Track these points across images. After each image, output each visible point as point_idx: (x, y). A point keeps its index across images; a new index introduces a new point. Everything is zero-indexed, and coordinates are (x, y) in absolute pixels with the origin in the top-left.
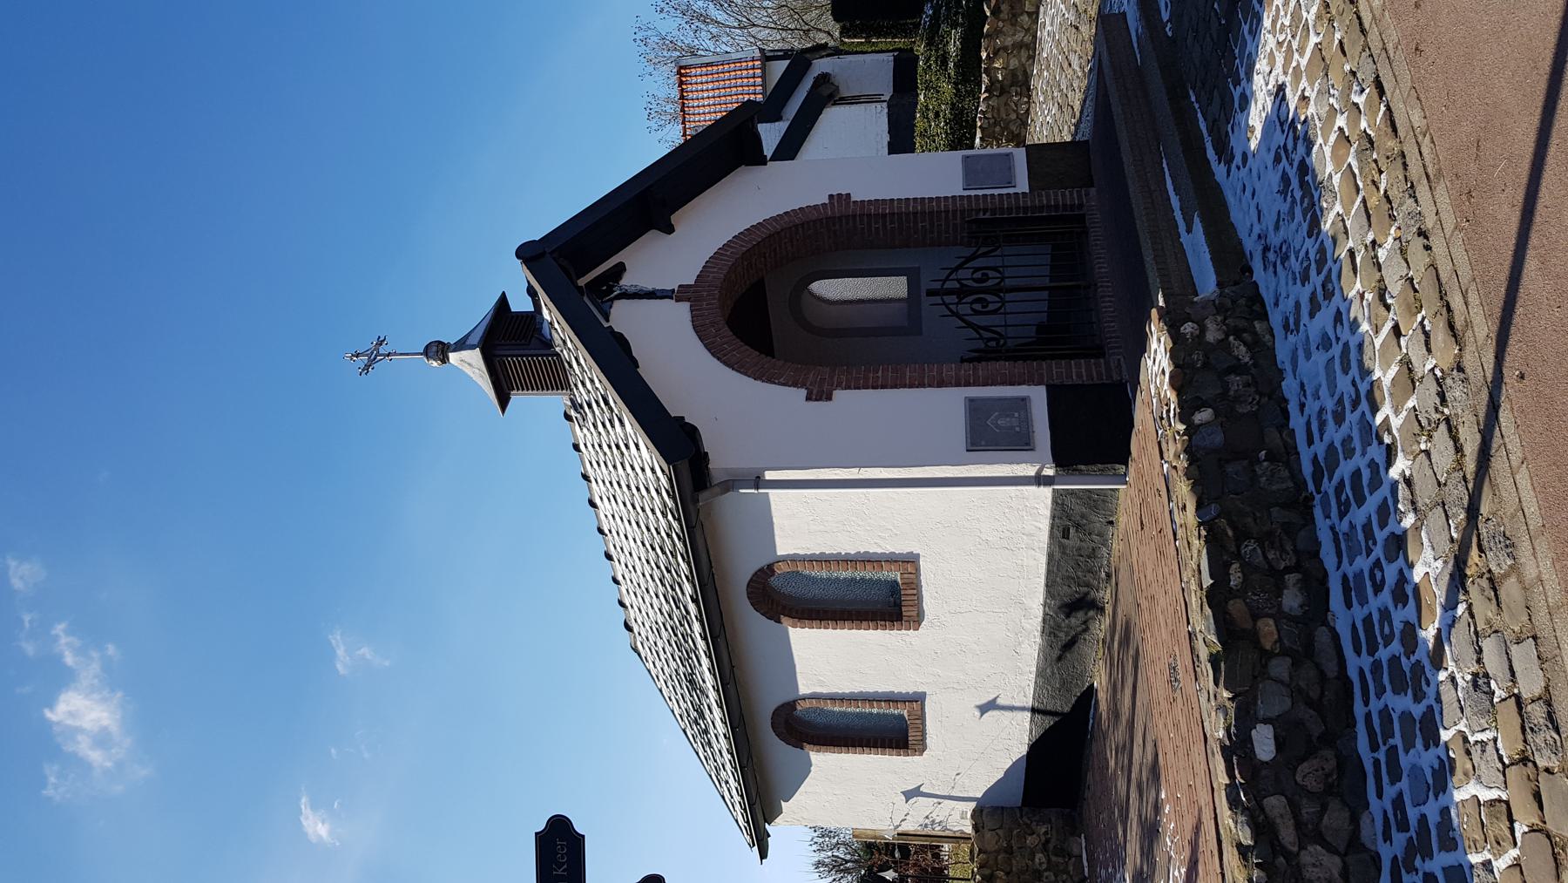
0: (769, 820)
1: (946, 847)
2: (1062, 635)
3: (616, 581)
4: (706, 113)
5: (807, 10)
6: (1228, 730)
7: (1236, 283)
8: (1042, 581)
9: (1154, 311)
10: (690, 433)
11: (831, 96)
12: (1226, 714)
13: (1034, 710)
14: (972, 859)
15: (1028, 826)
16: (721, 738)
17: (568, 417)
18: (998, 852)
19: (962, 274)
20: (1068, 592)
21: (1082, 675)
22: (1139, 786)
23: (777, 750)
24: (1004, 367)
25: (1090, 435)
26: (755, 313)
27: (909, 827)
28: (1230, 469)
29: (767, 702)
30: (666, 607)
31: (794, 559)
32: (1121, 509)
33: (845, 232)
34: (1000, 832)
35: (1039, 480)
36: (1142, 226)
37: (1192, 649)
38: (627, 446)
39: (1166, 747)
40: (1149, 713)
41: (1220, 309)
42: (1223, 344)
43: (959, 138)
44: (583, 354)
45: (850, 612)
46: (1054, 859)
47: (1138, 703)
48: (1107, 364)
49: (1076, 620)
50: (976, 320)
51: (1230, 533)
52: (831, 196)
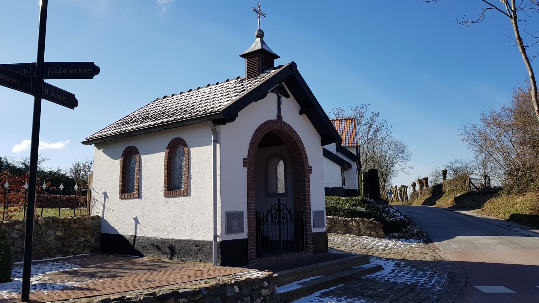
0: (96, 145)
1: (85, 209)
2: (162, 245)
3: (181, 93)
4: (339, 127)
5: (373, 161)
6: (129, 299)
7: (281, 299)
8: (181, 238)
9: (272, 272)
10: (232, 119)
11: (344, 168)
12: (135, 298)
13: (135, 236)
14: (82, 216)
15: (94, 235)
16: (126, 128)
17: (238, 78)
18: (85, 225)
19: (285, 210)
20: (177, 247)
21: (147, 252)
22: (108, 272)
23: (121, 148)
24: (254, 224)
25: (230, 253)
26: (273, 142)
27: (94, 194)
28: (219, 298)
29: (139, 145)
30: (172, 110)
31: (189, 154)
32: (205, 264)
33: (299, 172)
34: (91, 226)
35: (215, 236)
36: (300, 269)
37: (157, 287)
38: (228, 97)
39: (123, 280)
40: (135, 274)
41: (272, 294)
42: (260, 295)
43: (330, 211)
44: (259, 83)
45: (170, 173)
46: (82, 244)
47: (138, 271)
48: (254, 259)
49: (167, 250)
50: (270, 215)
51: (197, 298)
52: (311, 167)
